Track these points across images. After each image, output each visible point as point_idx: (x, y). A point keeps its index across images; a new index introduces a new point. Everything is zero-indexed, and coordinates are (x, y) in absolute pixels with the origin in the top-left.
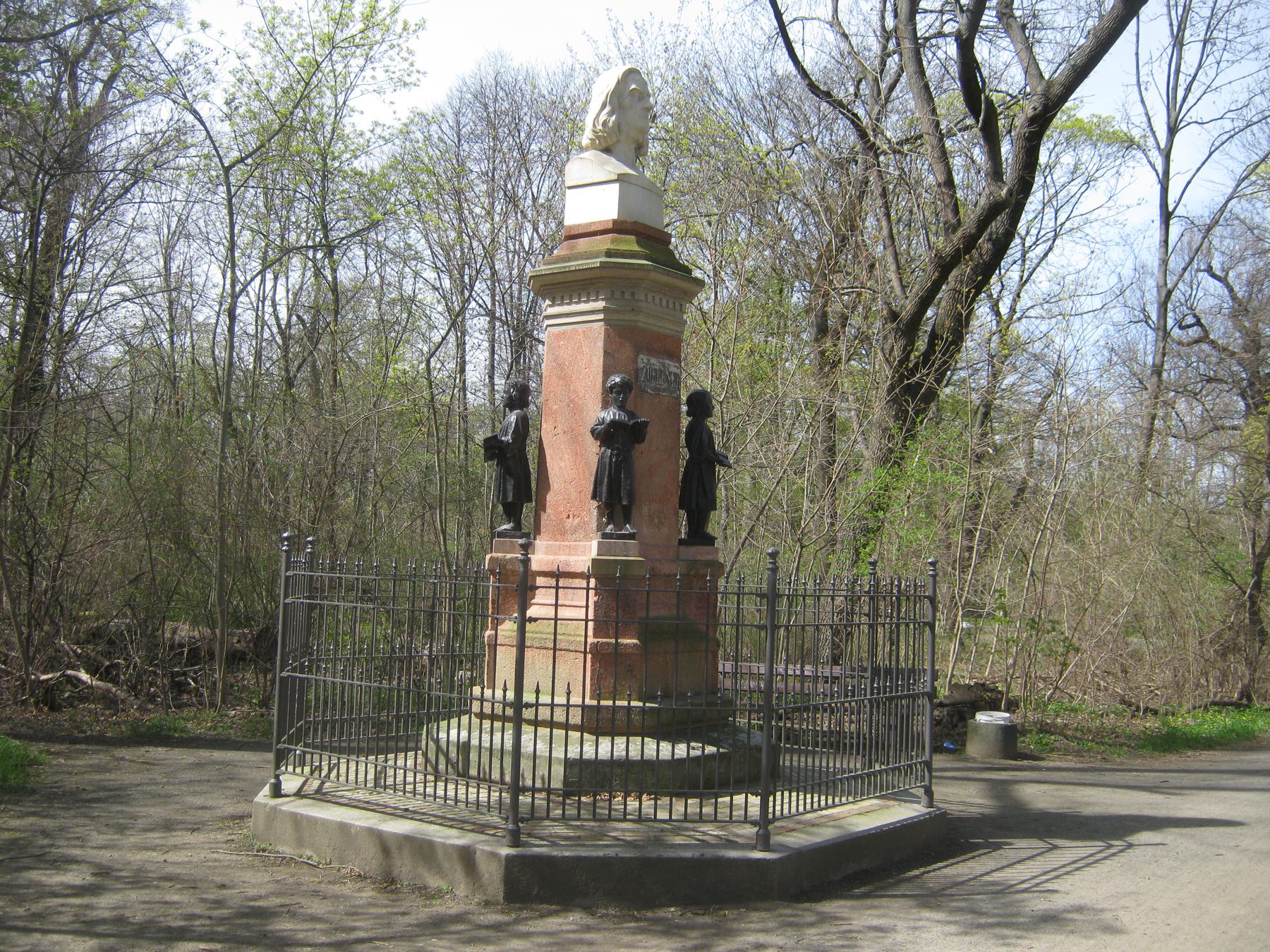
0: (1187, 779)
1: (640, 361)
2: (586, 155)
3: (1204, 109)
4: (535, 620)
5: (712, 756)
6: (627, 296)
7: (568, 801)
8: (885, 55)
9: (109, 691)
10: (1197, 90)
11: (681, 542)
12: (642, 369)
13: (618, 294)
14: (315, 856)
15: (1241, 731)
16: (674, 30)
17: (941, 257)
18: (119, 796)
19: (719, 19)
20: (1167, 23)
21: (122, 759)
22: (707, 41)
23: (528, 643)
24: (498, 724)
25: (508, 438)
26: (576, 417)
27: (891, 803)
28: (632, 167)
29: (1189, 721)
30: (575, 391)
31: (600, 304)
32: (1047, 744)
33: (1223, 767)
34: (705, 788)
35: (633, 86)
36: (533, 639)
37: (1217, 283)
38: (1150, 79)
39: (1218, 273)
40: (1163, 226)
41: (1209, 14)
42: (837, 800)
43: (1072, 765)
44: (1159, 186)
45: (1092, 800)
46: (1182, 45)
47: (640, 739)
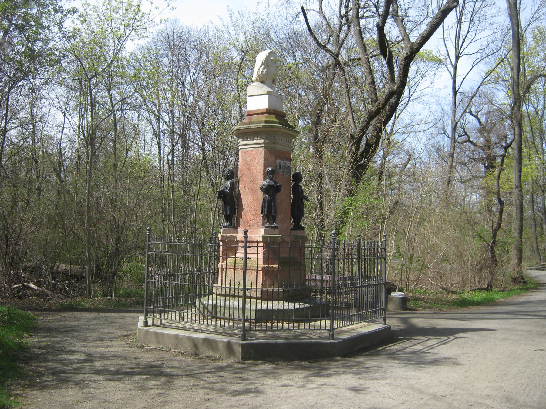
0: (472, 316)
2: (254, 84)
3: (469, 50)
4: (250, 258)
7: (257, 325)
8: (341, 26)
9: (43, 291)
10: (467, 41)
11: (292, 229)
13: (269, 137)
14: (164, 347)
15: (489, 299)
17: (370, 113)
18: (73, 330)
19: (273, 10)
20: (455, 14)
21: (65, 317)
22: (267, 19)
23: (247, 268)
24: (227, 298)
25: (227, 191)
26: (253, 183)
27: (371, 324)
28: (272, 88)
29: (469, 295)
30: (252, 173)
31: (262, 141)
32: (417, 305)
33: (484, 312)
34: (316, 317)
35: (272, 58)
36: (239, 266)
37: (473, 117)
38: (448, 36)
39: (474, 113)
40: (454, 97)
41: (472, 10)
42: (350, 323)
43: (428, 312)
44: (452, 80)
45: (439, 323)
46: (461, 23)
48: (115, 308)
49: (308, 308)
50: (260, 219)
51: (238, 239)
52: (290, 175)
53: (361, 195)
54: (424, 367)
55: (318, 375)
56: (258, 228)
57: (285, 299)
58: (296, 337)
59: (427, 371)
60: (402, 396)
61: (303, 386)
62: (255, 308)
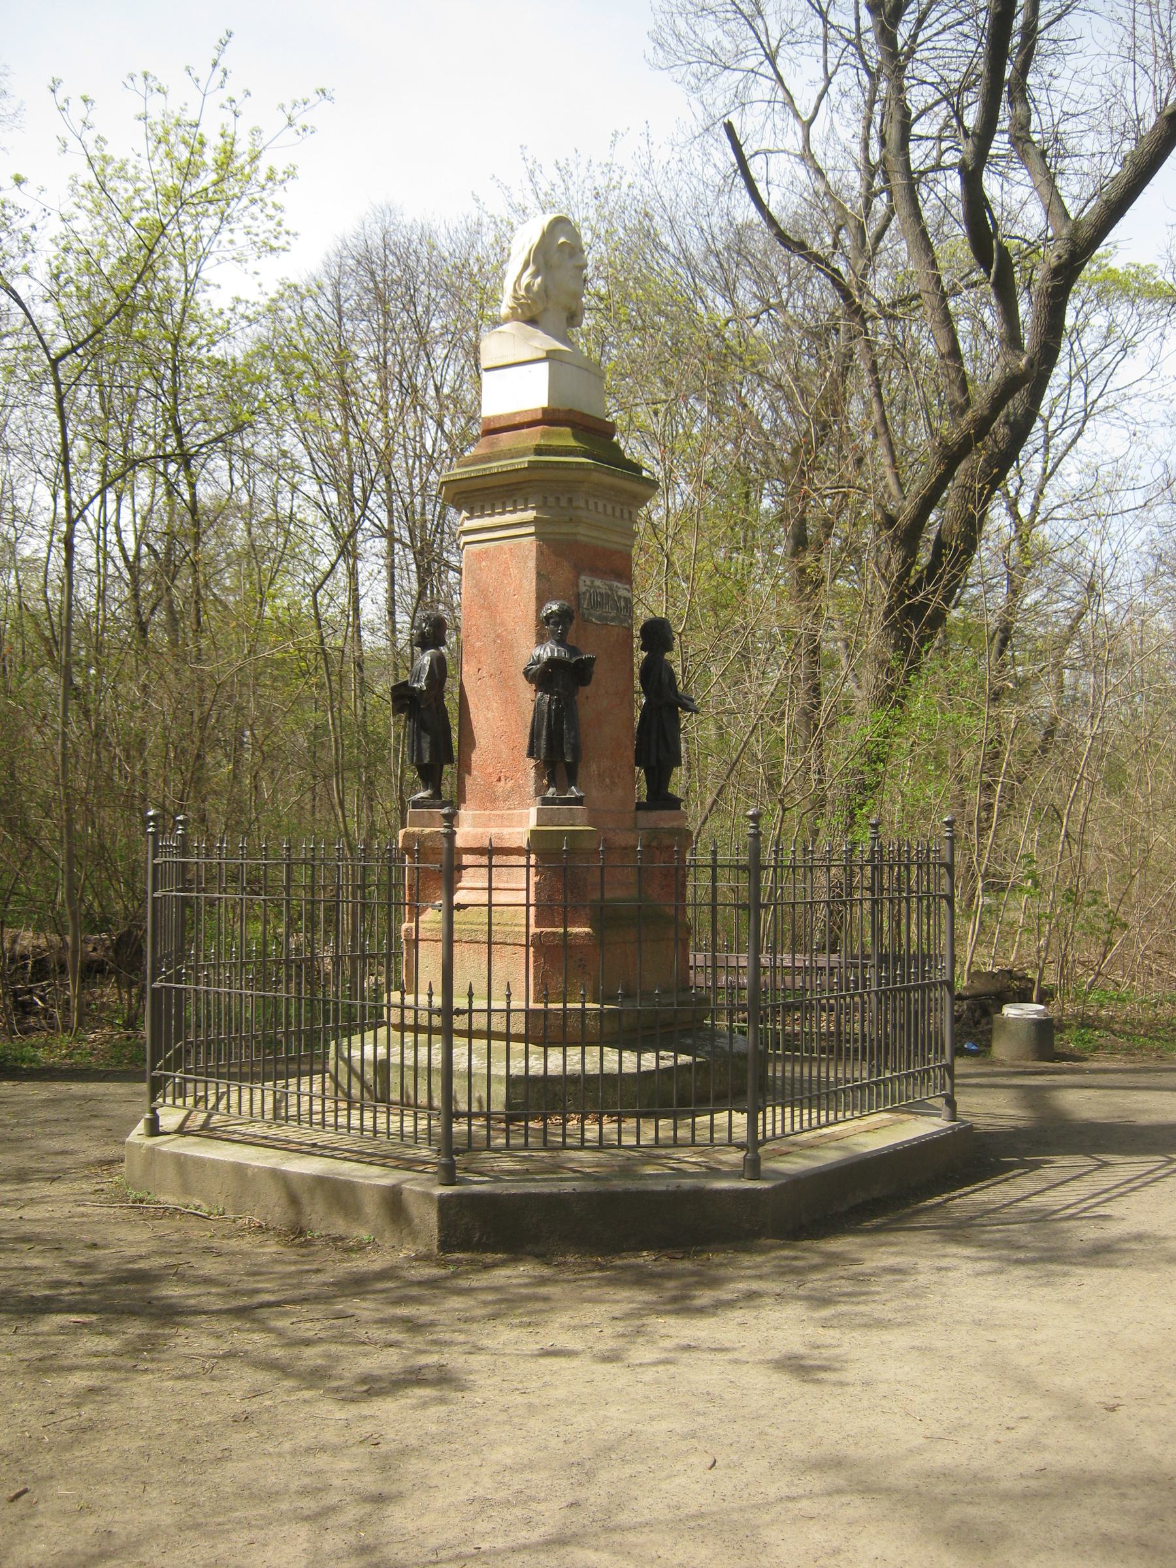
1: (581, 583)
2: (505, 328)
4: (465, 907)
11: (640, 806)
13: (551, 501)
17: (947, 446)
23: (455, 938)
24: (423, 1037)
25: (421, 685)
27: (905, 1117)
28: (565, 340)
30: (502, 624)
31: (531, 514)
35: (562, 240)
43: (1121, 1065)
48: (132, 1067)
49: (687, 1067)
50: (526, 775)
52: (630, 629)
53: (916, 706)
54: (1065, 1275)
55: (681, 1306)
56: (523, 805)
57: (622, 1043)
58: (626, 1171)
59: (1071, 1295)
60: (953, 1405)
61: (610, 1358)
62: (503, 1073)
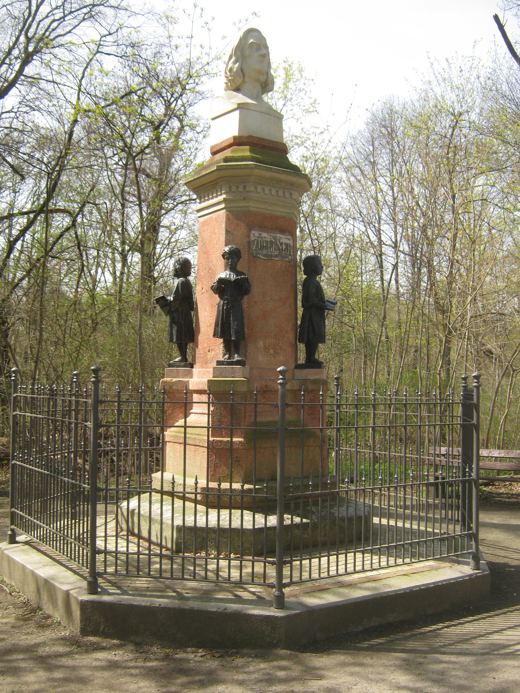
1: (252, 235)
5: (297, 526)
6: (241, 189)
11: (299, 367)
12: (254, 241)
13: (234, 188)
16: (470, 59)
30: (212, 262)
31: (221, 198)
35: (251, 41)
47: (239, 511)
50: (219, 348)
51: (191, 387)
